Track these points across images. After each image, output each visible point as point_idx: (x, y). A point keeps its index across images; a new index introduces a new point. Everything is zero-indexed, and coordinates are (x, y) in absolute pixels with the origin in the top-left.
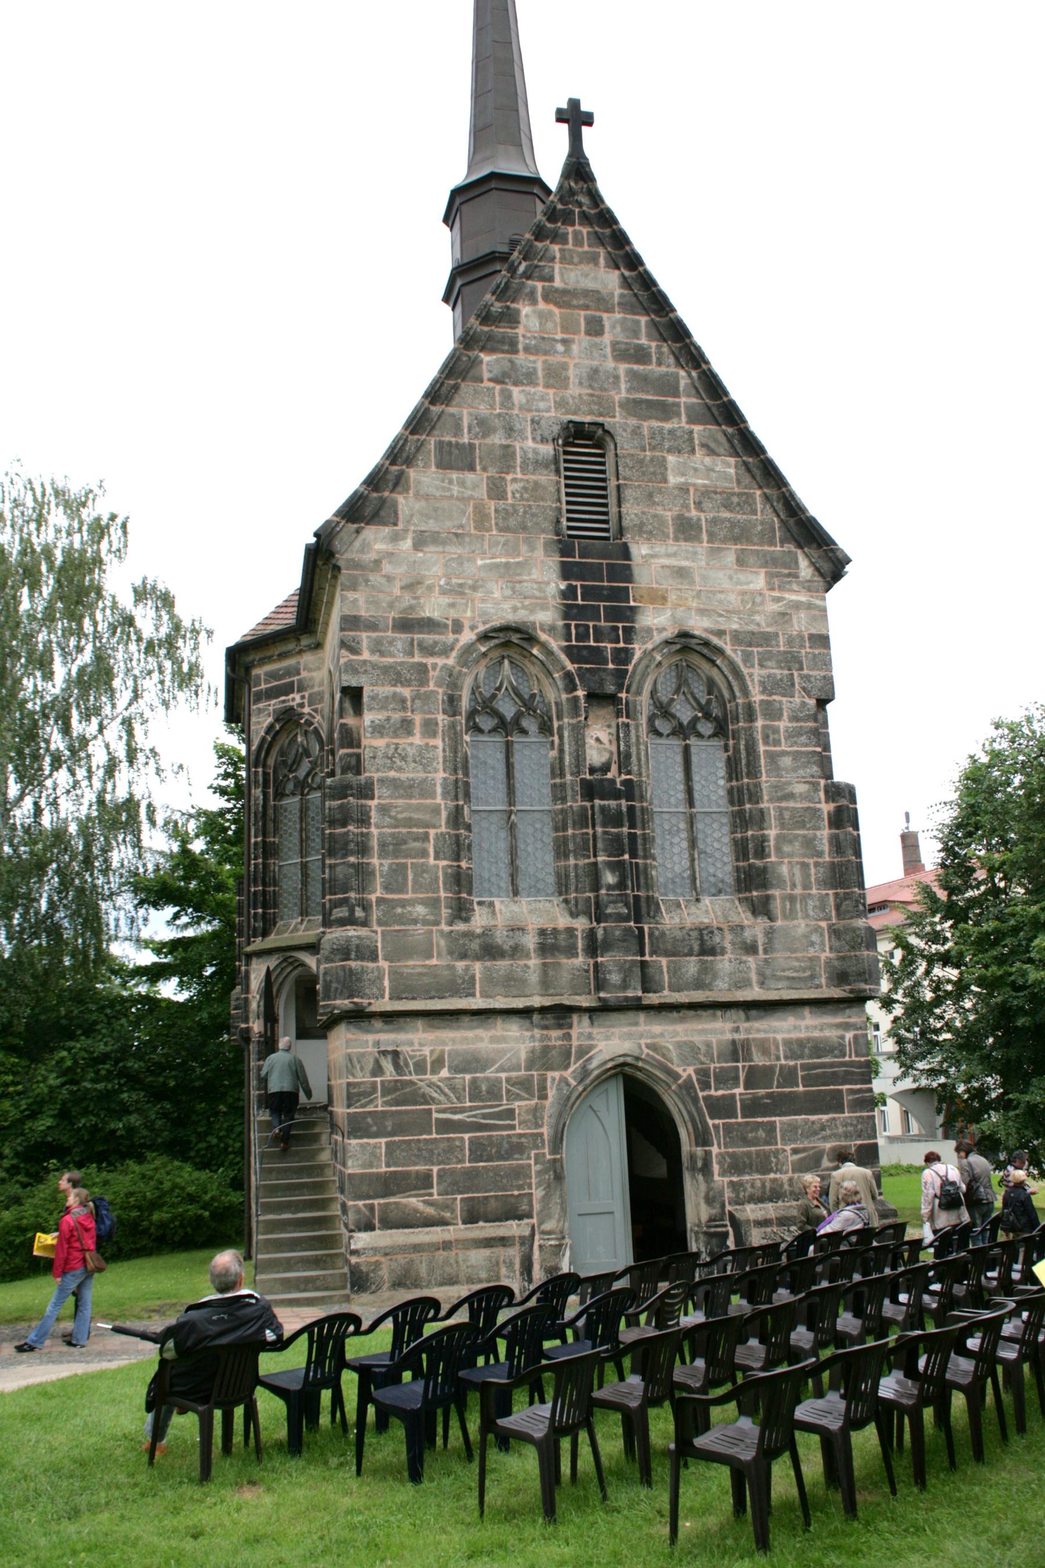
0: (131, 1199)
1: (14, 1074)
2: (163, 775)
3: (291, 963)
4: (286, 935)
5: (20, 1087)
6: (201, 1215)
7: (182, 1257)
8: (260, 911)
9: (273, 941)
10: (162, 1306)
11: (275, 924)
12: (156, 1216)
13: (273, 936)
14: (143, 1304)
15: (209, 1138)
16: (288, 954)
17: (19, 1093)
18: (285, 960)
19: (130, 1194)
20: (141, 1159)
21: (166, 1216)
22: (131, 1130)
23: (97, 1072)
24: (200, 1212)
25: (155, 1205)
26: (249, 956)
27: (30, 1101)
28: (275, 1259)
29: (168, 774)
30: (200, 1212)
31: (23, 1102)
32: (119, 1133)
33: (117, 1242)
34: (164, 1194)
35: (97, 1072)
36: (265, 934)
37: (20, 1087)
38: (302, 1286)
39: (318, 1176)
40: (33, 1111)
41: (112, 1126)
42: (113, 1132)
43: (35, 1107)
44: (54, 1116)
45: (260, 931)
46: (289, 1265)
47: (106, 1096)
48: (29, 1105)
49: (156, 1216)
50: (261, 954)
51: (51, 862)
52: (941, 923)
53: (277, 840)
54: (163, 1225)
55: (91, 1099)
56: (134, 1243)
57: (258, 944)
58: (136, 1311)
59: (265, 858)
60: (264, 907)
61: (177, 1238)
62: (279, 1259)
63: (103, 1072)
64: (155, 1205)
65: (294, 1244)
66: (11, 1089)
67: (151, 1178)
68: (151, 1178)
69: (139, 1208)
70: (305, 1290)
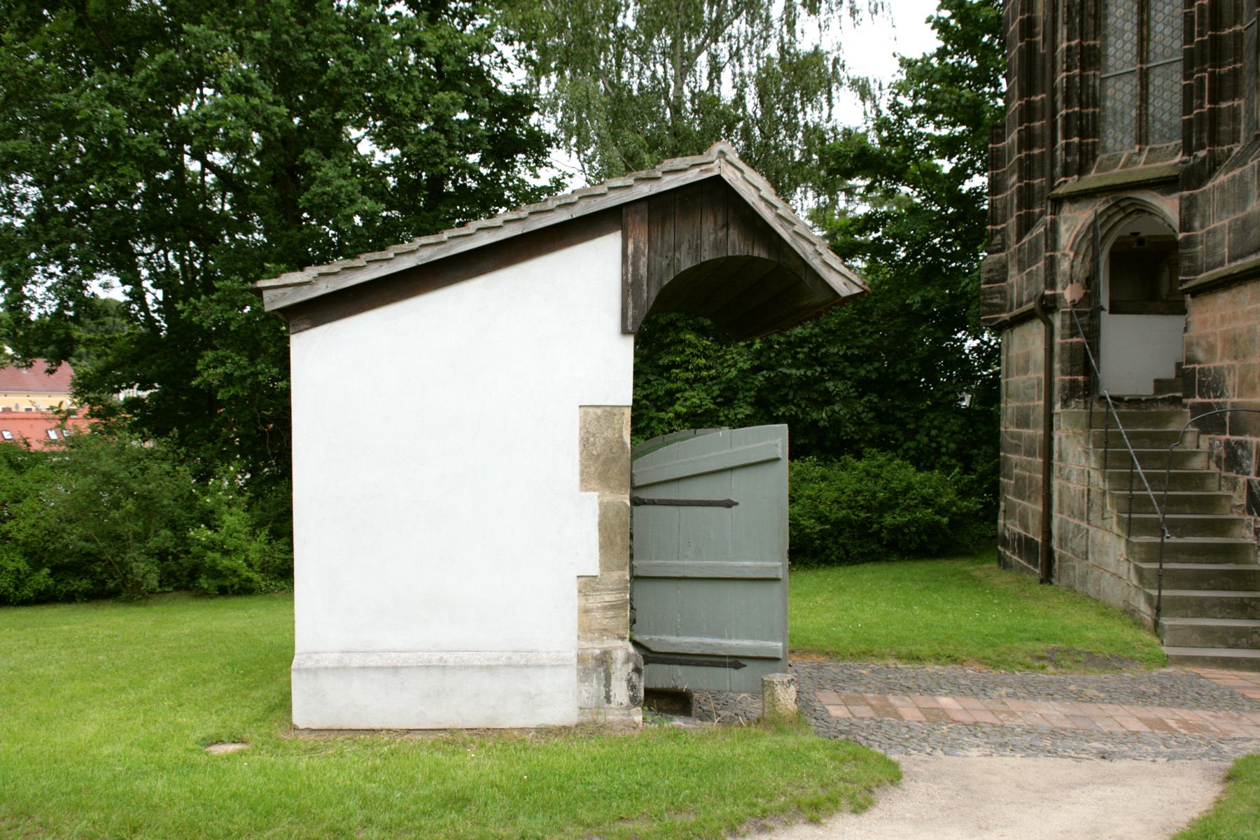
0: (859, 498)
1: (707, 357)
2: (857, 17)
3: (1123, 209)
4: (1116, 170)
5: (713, 372)
6: (938, 523)
7: (921, 568)
8: (1076, 140)
9: (1093, 179)
10: (1054, 651)
11: (1094, 157)
12: (888, 519)
13: (1093, 173)
14: (1030, 646)
15: (918, 437)
16: (1125, 195)
17: (712, 378)
18: (1116, 204)
19: (857, 492)
20: (859, 456)
21: (900, 520)
22: (835, 423)
23: (794, 357)
24: (937, 517)
25: (885, 507)
26: (1058, 202)
27: (722, 386)
28: (1181, 599)
29: (864, 14)
30: (937, 517)
31: (715, 388)
32: (821, 423)
33: (843, 545)
34: (895, 494)
35: (794, 357)
36: (1082, 170)
37: (713, 372)
38: (1231, 641)
39: (1197, 488)
40: (725, 398)
41: (815, 415)
42: (815, 422)
43: (728, 394)
44: (751, 404)
45: (1076, 166)
46: (1201, 608)
47: (805, 384)
48: (722, 391)
49: (888, 519)
50: (1076, 198)
51: (739, 120)
52: (844, 367)
53: (1098, 43)
54: (896, 529)
55: (790, 387)
56: (861, 546)
57: (1072, 184)
58: (1020, 656)
59: (1083, 69)
60: (1081, 136)
61: (913, 546)
62: (1187, 599)
63: (801, 356)
64: (885, 507)
65: (1198, 580)
66: (705, 373)
67: (877, 476)
68: (877, 476)
69: (868, 508)
70: (1235, 646)
